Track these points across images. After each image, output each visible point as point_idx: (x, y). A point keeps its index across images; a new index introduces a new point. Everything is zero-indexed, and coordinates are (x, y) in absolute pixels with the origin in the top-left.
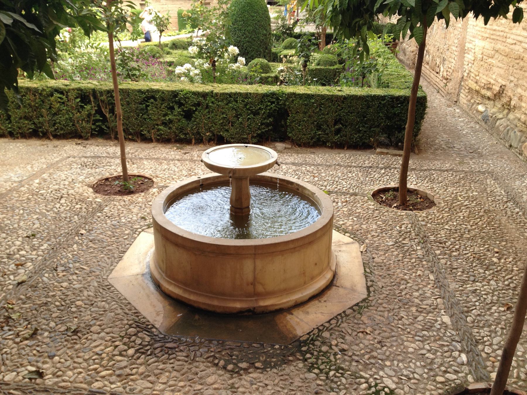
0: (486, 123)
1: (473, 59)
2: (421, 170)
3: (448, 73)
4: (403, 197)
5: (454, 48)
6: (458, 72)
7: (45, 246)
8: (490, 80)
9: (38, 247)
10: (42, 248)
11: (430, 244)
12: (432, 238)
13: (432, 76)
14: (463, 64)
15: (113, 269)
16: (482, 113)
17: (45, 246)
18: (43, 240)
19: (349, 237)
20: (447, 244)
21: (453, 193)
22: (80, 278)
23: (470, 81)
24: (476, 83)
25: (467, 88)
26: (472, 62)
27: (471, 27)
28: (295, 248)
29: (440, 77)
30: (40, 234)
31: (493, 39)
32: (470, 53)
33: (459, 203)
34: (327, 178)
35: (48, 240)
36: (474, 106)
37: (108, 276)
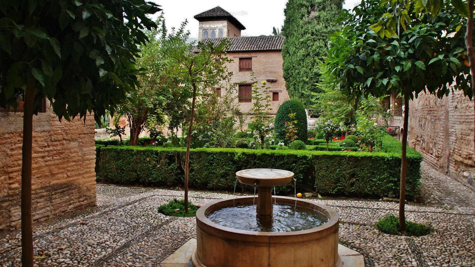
0: (471, 184)
1: (455, 139)
2: (419, 212)
3: (439, 153)
4: (400, 227)
5: (441, 134)
6: (446, 150)
7: (124, 240)
8: (469, 151)
9: (119, 241)
10: (121, 241)
11: (424, 258)
12: (425, 254)
13: (428, 157)
14: (449, 144)
15: (165, 258)
16: (467, 177)
17: (124, 240)
18: (123, 237)
19: (356, 251)
20: (438, 258)
21: (444, 227)
22: (141, 261)
23: (455, 155)
24: (460, 156)
25: (454, 161)
26: (455, 141)
27: (451, 117)
28: (303, 242)
29: (433, 157)
30: (122, 234)
31: (468, 122)
32: (453, 135)
33: (449, 233)
34: (343, 214)
35: (127, 238)
36: (461, 173)
37: (161, 262)
